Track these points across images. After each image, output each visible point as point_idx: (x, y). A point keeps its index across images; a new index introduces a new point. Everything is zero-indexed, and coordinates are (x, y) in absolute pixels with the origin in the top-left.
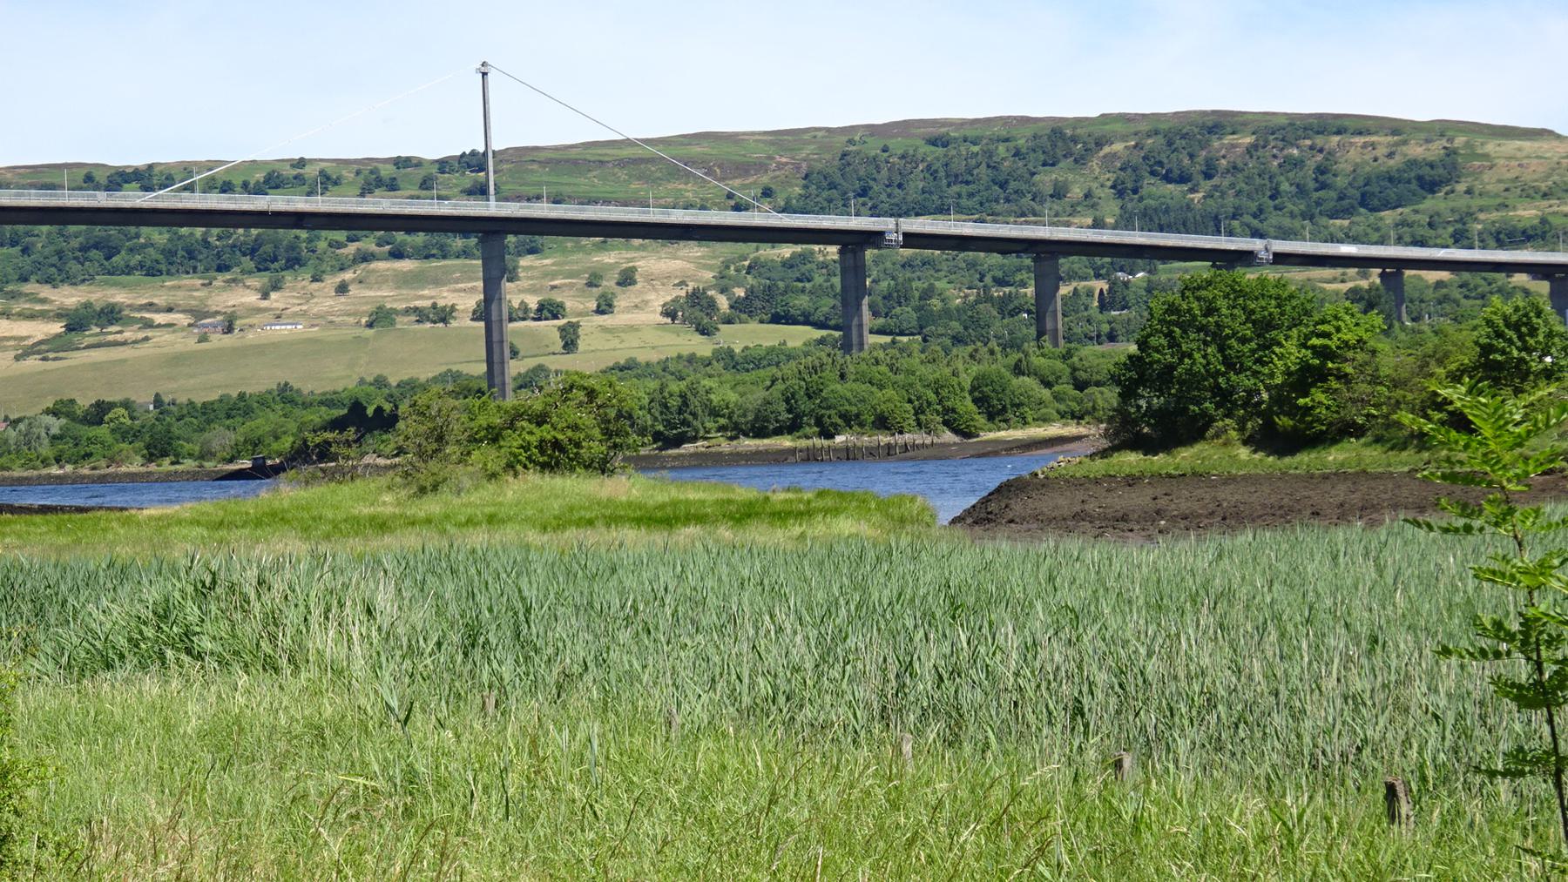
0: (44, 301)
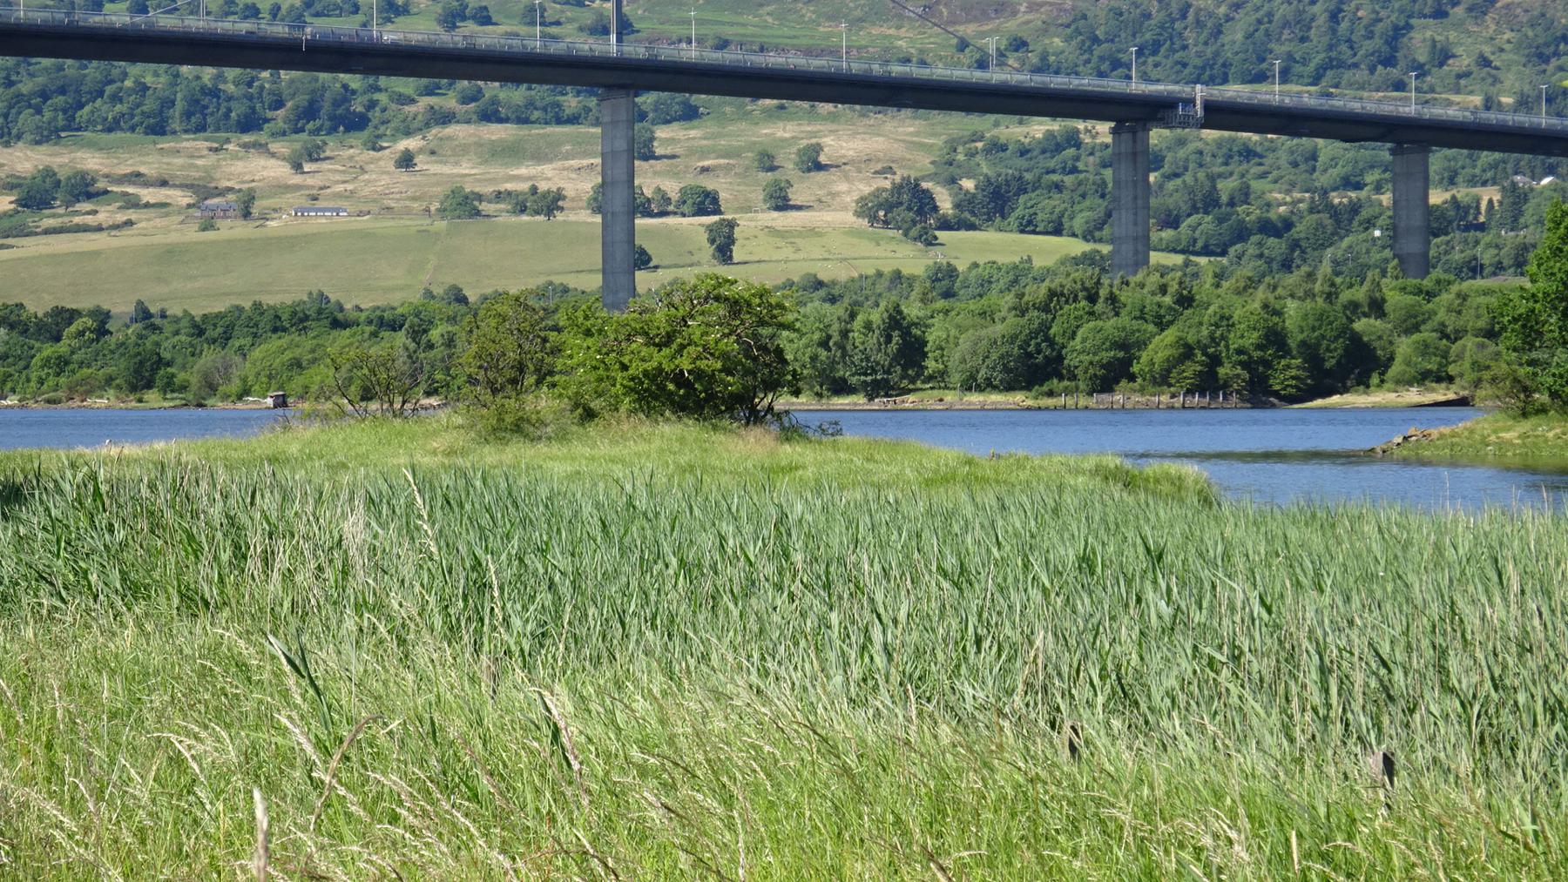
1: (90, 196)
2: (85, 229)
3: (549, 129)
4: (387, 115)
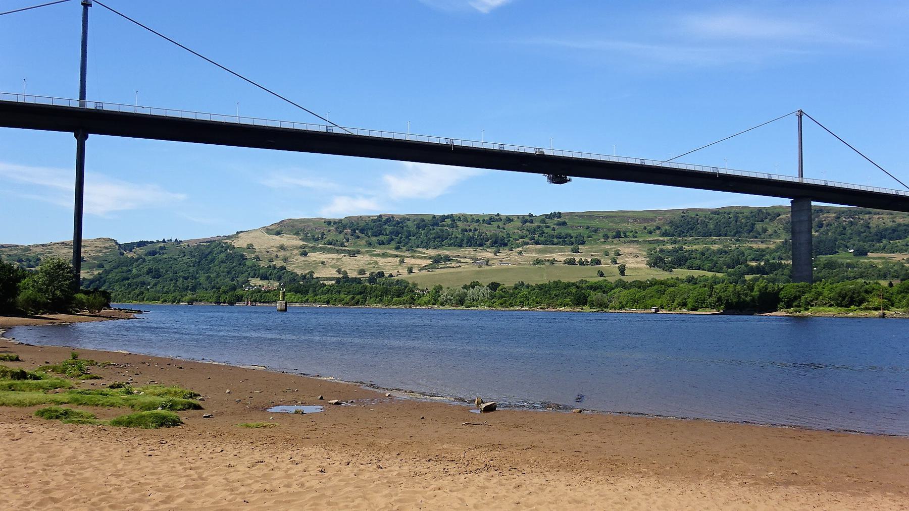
0: (424, 253)
1: (449, 260)
2: (450, 267)
3: (552, 246)
4: (513, 243)
